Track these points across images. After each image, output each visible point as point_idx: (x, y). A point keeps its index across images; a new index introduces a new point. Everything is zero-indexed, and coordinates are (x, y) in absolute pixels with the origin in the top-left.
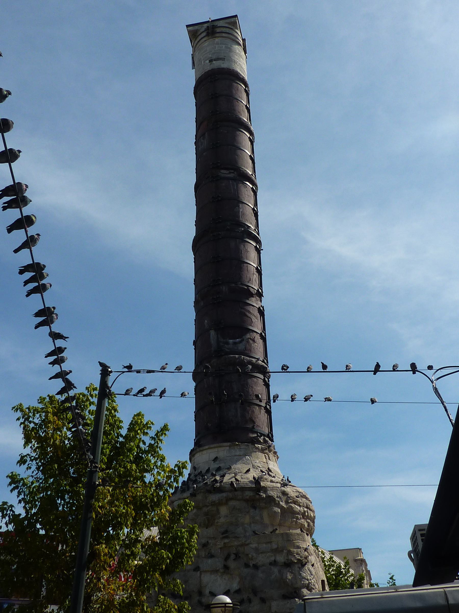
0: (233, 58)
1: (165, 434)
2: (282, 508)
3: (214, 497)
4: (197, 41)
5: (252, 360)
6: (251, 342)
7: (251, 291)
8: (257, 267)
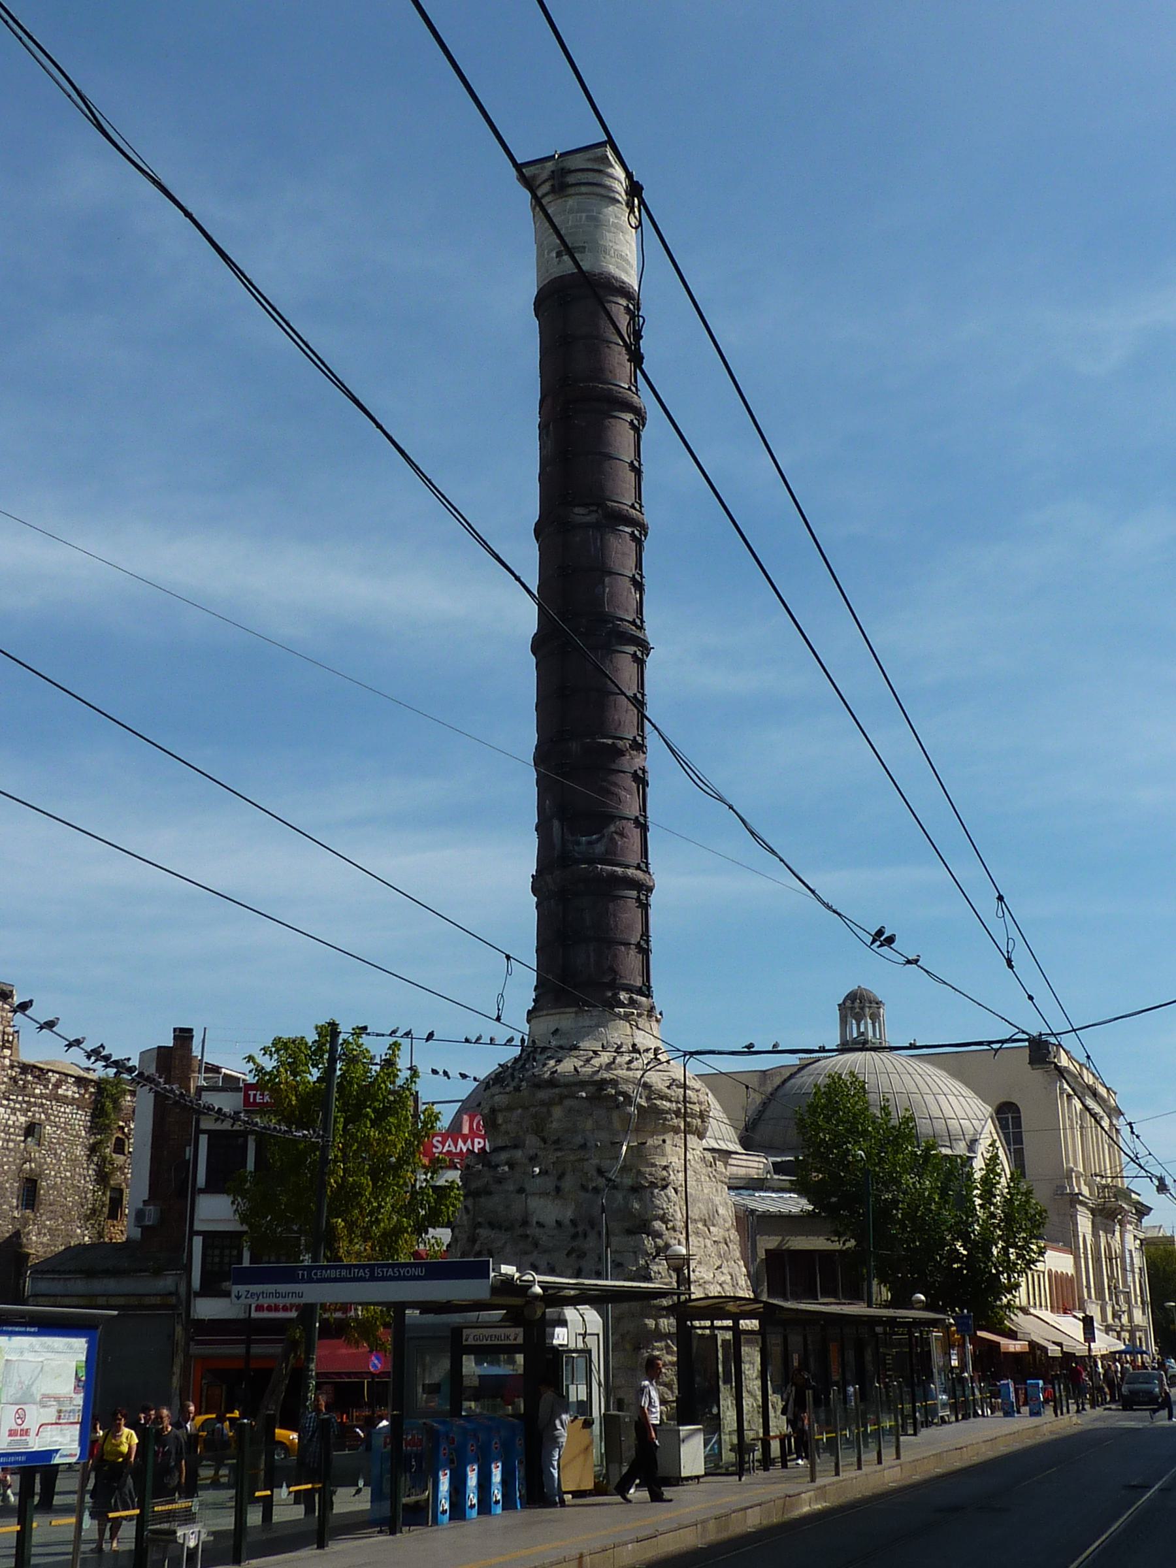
0: (602, 243)
1: (415, 1082)
2: (639, 1107)
3: (542, 1095)
5: (615, 871)
6: (617, 837)
7: (619, 746)
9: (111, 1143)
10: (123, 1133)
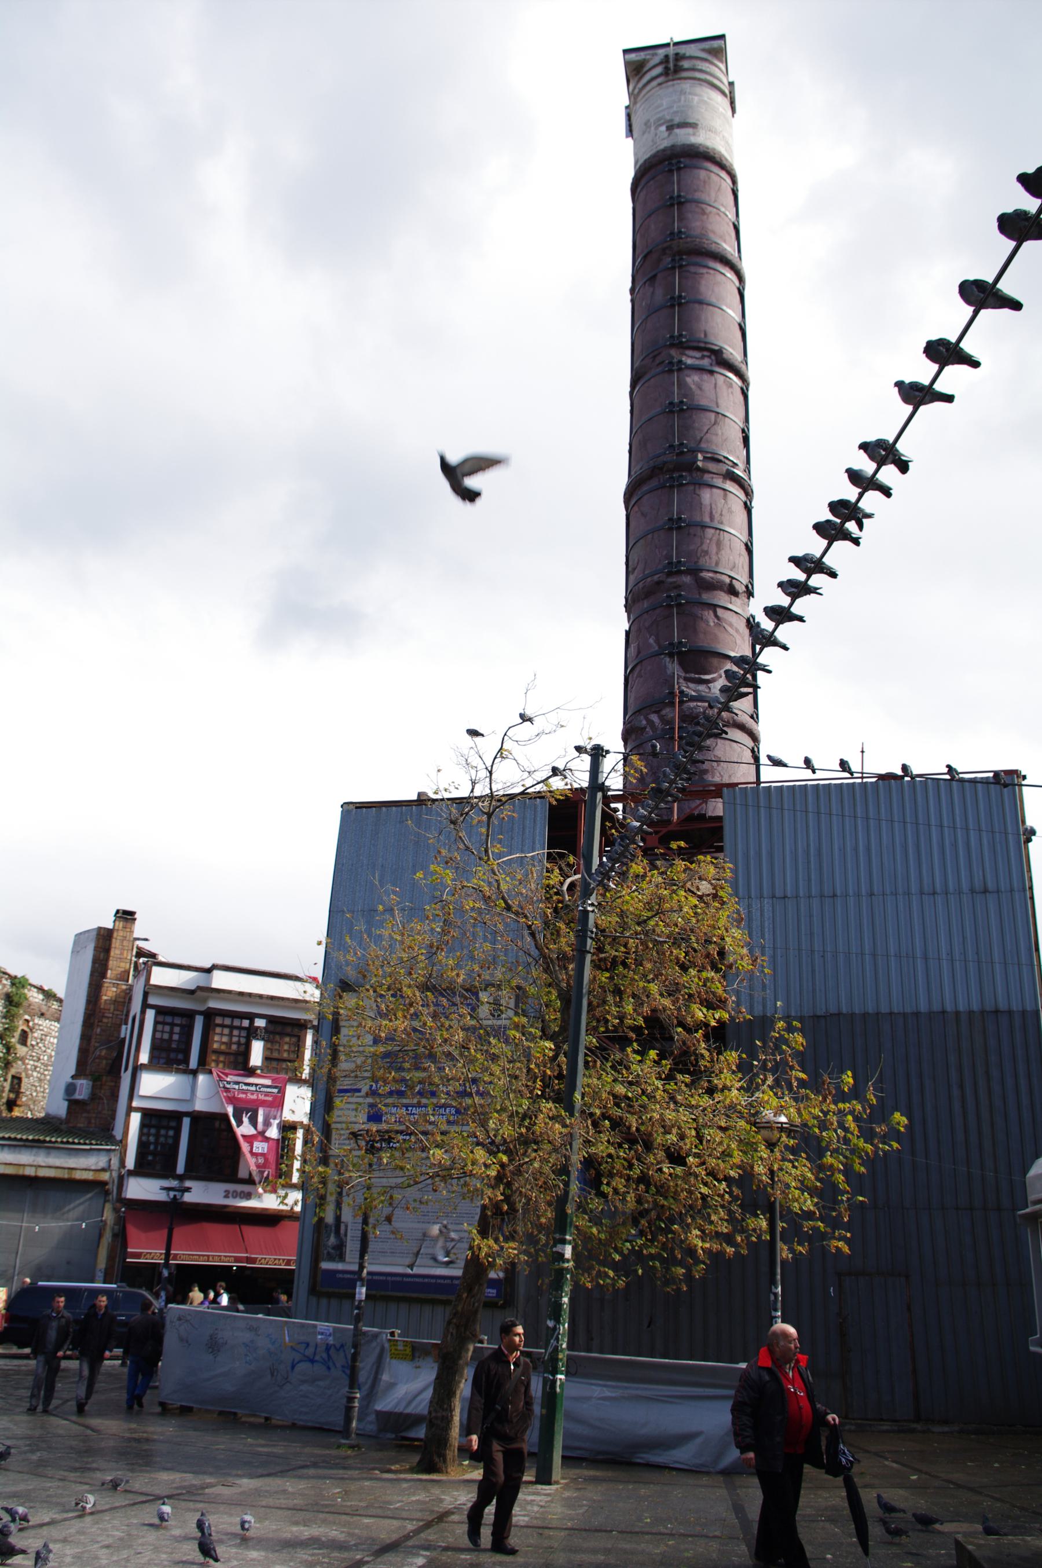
4: (640, 85)
8: (753, 748)
9: (17, 1034)
10: (28, 1026)
